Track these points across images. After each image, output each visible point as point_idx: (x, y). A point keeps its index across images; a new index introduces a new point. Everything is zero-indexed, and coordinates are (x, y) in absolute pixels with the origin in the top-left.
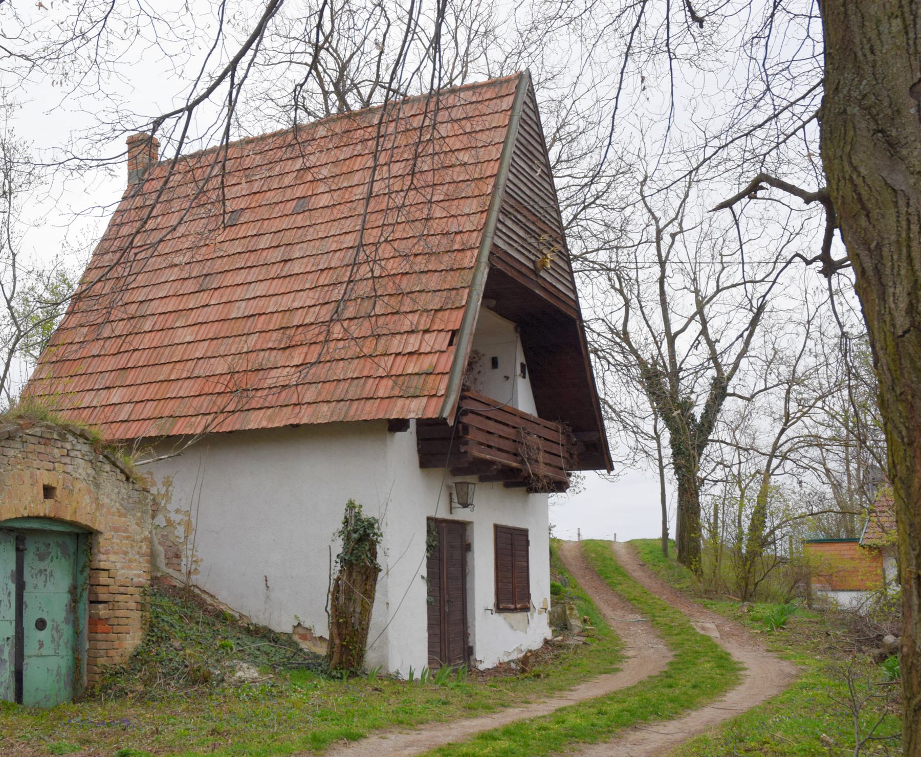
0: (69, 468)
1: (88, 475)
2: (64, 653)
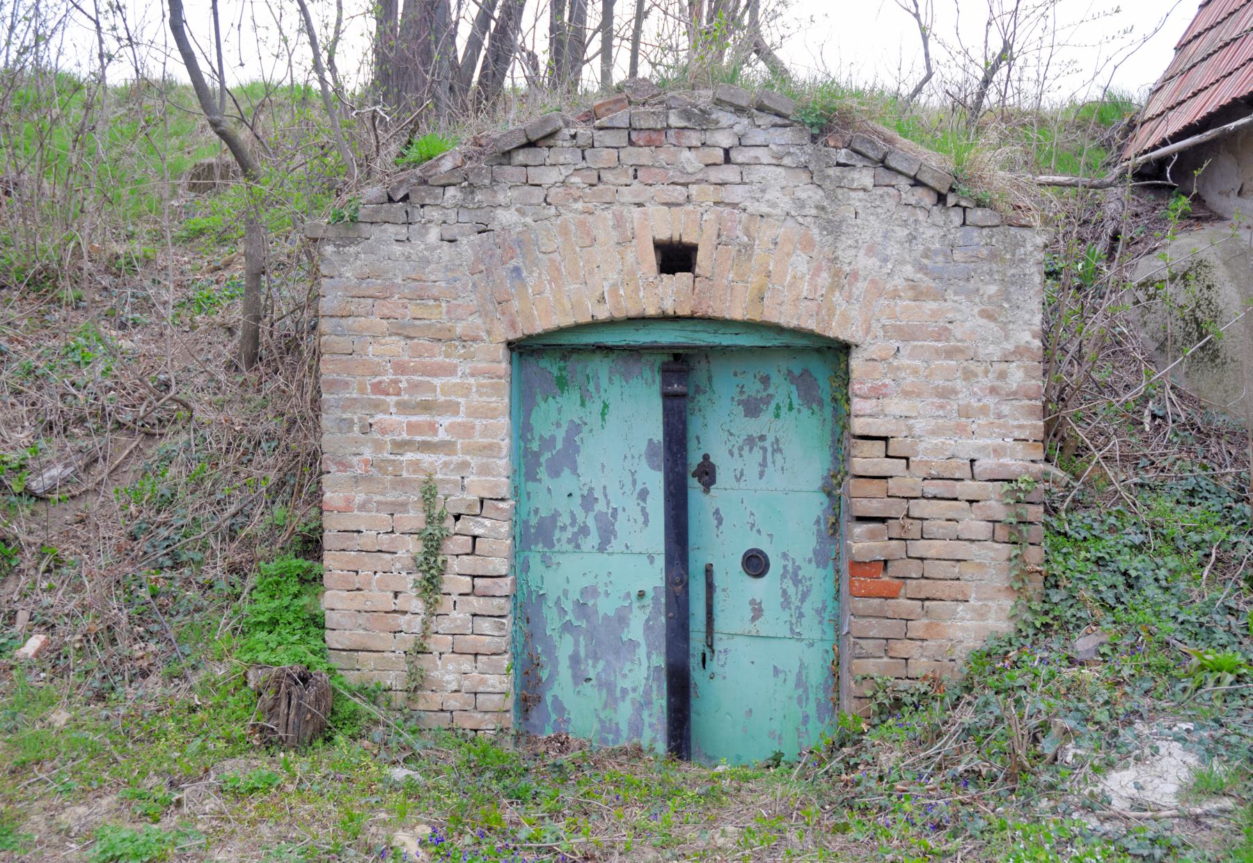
0: (736, 194)
1: (800, 204)
2: (816, 634)
